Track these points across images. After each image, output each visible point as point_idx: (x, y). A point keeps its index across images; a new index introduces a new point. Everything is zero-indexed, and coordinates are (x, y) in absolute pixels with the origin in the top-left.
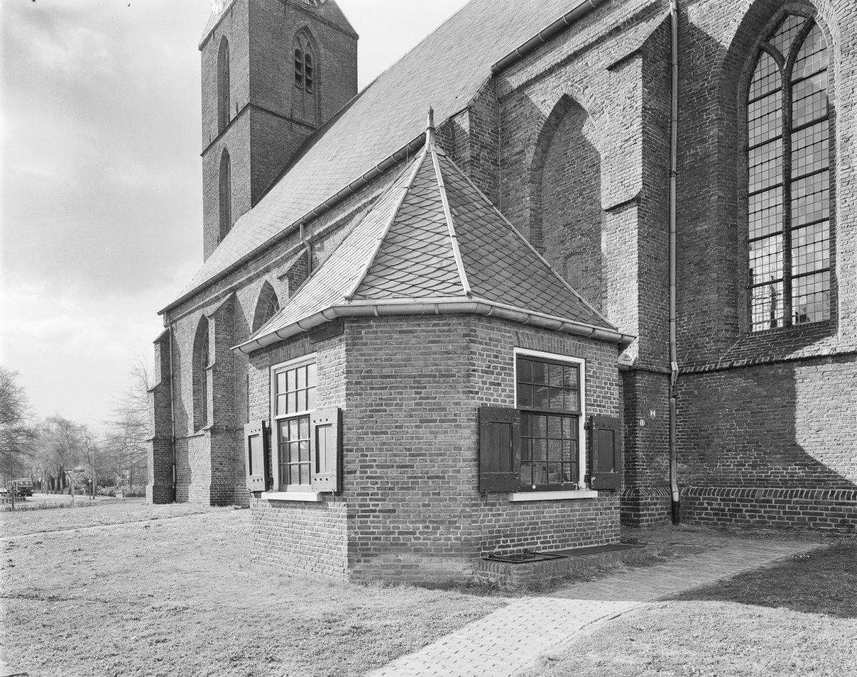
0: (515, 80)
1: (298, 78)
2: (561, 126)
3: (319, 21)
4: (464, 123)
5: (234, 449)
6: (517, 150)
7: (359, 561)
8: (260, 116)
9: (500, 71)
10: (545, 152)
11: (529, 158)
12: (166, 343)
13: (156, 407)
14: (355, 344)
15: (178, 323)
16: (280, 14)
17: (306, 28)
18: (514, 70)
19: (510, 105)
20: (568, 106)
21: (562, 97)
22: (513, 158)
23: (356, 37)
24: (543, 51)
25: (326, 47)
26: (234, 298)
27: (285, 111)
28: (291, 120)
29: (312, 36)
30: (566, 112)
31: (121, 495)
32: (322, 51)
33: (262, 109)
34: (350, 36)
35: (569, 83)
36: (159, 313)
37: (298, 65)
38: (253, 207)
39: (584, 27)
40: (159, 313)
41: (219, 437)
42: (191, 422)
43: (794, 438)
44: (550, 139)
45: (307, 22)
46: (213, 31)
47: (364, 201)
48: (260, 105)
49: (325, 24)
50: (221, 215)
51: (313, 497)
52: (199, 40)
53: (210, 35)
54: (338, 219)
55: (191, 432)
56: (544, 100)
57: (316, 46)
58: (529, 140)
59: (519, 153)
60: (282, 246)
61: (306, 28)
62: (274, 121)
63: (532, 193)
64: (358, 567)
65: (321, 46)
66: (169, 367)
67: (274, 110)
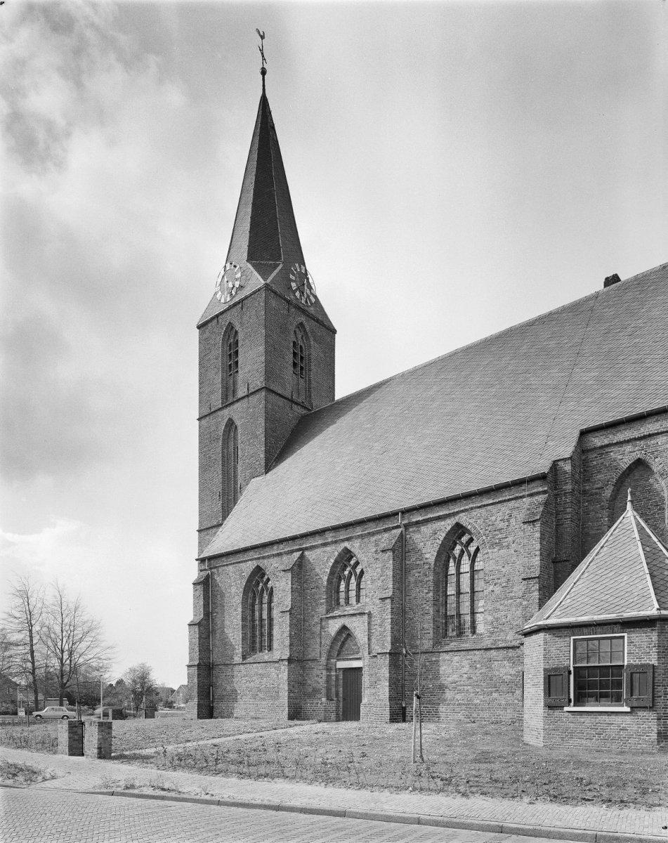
0: (597, 441)
1: (295, 365)
2: (631, 476)
3: (311, 318)
4: (567, 467)
5: (302, 675)
6: (598, 486)
7: (662, 742)
8: (272, 397)
9: (584, 433)
10: (618, 490)
11: (608, 493)
12: (206, 586)
13: (200, 638)
14: (663, 633)
15: (220, 569)
16: (285, 312)
17: (301, 324)
18: (597, 434)
19: (592, 456)
20: (640, 464)
21: (637, 460)
22: (594, 491)
23: (334, 331)
24: (623, 428)
25: (315, 340)
26: (302, 557)
27: (288, 394)
28: (292, 401)
29: (305, 331)
30: (636, 468)
31: (24, 713)
32: (312, 343)
33: (273, 392)
34: (331, 331)
35: (643, 452)
36: (197, 560)
37: (295, 354)
38: (268, 469)
39: (657, 421)
40: (197, 560)
41: (292, 666)
42: (239, 650)
43: (392, 647)
44: (622, 482)
45: (303, 319)
46: (217, 316)
47: (471, 506)
48: (271, 388)
49: (314, 320)
50: (223, 474)
51: (628, 709)
52: (197, 319)
53: (212, 319)
54: (441, 514)
55: (238, 659)
56: (624, 456)
57: (307, 338)
58: (608, 481)
59: (599, 488)
60: (371, 524)
61: (301, 324)
62: (281, 402)
63: (608, 517)
64: (661, 745)
65: (312, 339)
66: (209, 605)
67: (279, 392)
